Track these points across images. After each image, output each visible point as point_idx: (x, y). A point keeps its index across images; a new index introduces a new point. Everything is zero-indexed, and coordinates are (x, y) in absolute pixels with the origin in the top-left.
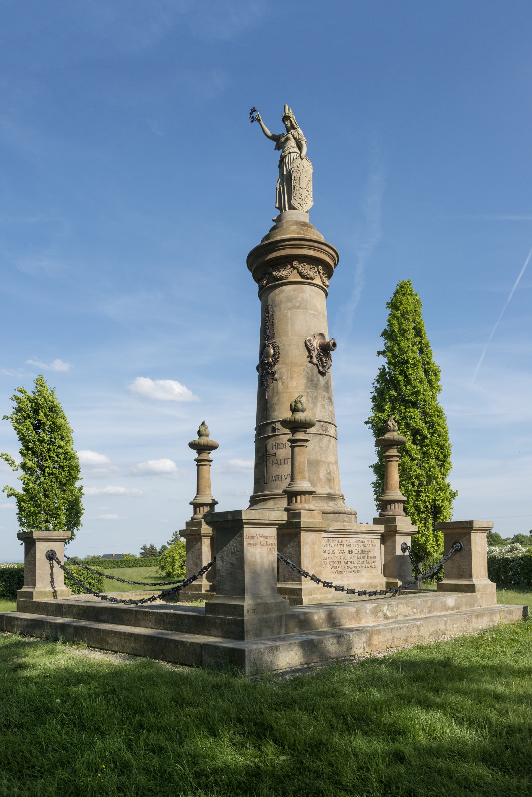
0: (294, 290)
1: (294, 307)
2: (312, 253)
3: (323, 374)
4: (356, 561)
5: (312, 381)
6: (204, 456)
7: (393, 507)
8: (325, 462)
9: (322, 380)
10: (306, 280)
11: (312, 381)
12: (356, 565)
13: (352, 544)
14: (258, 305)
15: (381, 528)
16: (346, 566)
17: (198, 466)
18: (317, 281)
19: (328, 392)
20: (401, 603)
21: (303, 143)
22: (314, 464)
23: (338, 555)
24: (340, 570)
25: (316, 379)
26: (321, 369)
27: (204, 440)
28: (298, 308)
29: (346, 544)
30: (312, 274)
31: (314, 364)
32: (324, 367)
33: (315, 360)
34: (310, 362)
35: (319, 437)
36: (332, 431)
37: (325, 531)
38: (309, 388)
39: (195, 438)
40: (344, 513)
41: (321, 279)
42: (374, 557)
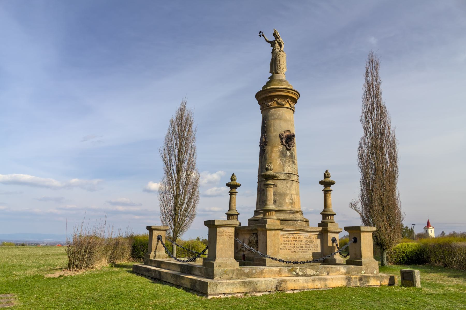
0: (275, 111)
1: (274, 119)
2: (283, 93)
3: (288, 150)
4: (304, 246)
5: (283, 153)
6: (234, 190)
7: (327, 218)
8: (289, 194)
9: (289, 154)
10: (281, 106)
11: (283, 153)
12: (304, 248)
13: (302, 237)
14: (260, 116)
15: (320, 229)
16: (298, 248)
17: (231, 195)
18: (287, 105)
19: (292, 158)
20: (308, 268)
21: (282, 44)
22: (283, 195)
23: (293, 242)
24: (294, 250)
25: (285, 152)
26: (288, 147)
27: (234, 182)
28: (277, 119)
29: (298, 237)
30: (284, 103)
31: (284, 145)
32: (289, 146)
33: (284, 143)
34: (282, 144)
35: (286, 181)
36: (294, 178)
37: (281, 230)
38: (281, 157)
39: (229, 181)
40: (296, 221)
41: (289, 104)
42: (317, 245)
